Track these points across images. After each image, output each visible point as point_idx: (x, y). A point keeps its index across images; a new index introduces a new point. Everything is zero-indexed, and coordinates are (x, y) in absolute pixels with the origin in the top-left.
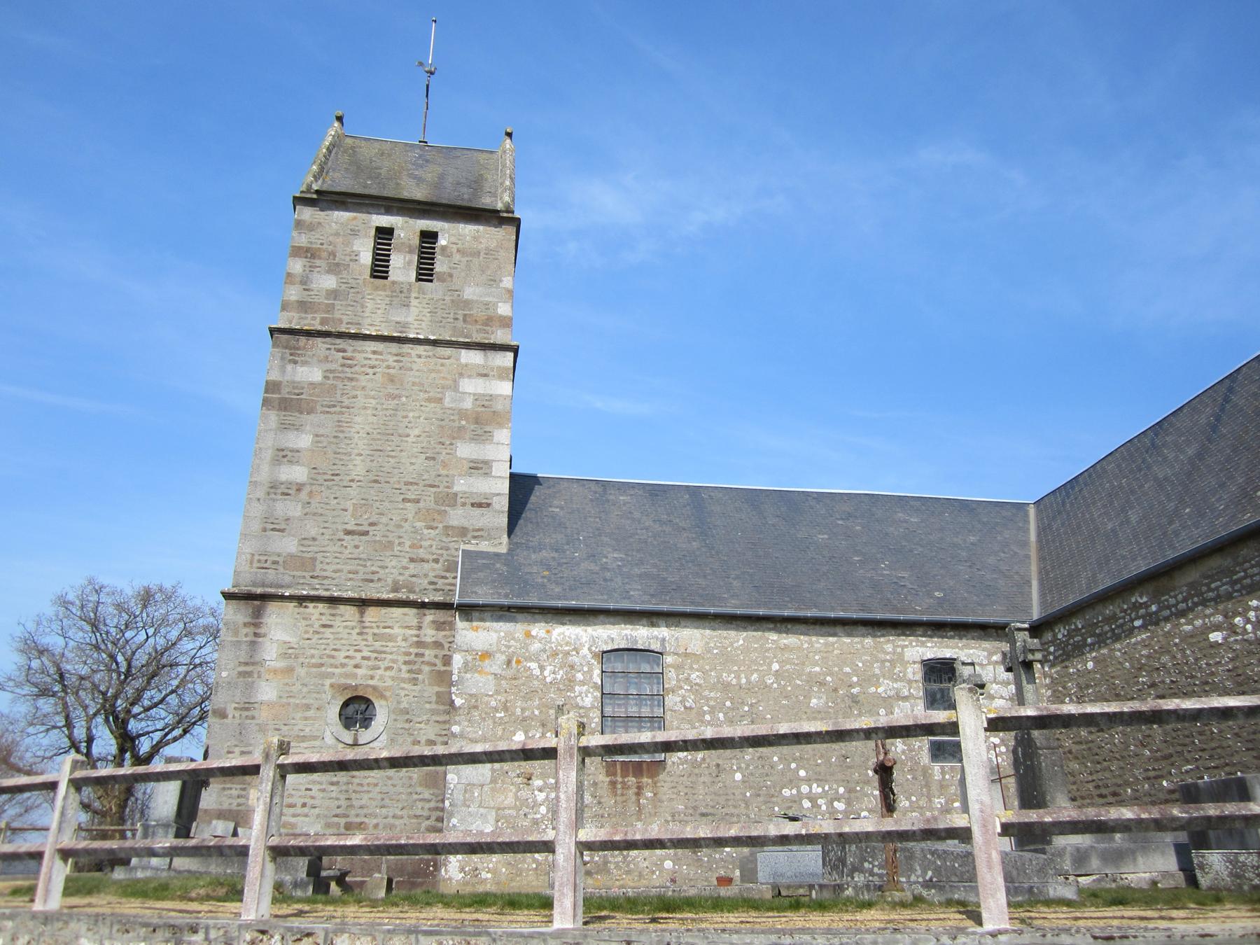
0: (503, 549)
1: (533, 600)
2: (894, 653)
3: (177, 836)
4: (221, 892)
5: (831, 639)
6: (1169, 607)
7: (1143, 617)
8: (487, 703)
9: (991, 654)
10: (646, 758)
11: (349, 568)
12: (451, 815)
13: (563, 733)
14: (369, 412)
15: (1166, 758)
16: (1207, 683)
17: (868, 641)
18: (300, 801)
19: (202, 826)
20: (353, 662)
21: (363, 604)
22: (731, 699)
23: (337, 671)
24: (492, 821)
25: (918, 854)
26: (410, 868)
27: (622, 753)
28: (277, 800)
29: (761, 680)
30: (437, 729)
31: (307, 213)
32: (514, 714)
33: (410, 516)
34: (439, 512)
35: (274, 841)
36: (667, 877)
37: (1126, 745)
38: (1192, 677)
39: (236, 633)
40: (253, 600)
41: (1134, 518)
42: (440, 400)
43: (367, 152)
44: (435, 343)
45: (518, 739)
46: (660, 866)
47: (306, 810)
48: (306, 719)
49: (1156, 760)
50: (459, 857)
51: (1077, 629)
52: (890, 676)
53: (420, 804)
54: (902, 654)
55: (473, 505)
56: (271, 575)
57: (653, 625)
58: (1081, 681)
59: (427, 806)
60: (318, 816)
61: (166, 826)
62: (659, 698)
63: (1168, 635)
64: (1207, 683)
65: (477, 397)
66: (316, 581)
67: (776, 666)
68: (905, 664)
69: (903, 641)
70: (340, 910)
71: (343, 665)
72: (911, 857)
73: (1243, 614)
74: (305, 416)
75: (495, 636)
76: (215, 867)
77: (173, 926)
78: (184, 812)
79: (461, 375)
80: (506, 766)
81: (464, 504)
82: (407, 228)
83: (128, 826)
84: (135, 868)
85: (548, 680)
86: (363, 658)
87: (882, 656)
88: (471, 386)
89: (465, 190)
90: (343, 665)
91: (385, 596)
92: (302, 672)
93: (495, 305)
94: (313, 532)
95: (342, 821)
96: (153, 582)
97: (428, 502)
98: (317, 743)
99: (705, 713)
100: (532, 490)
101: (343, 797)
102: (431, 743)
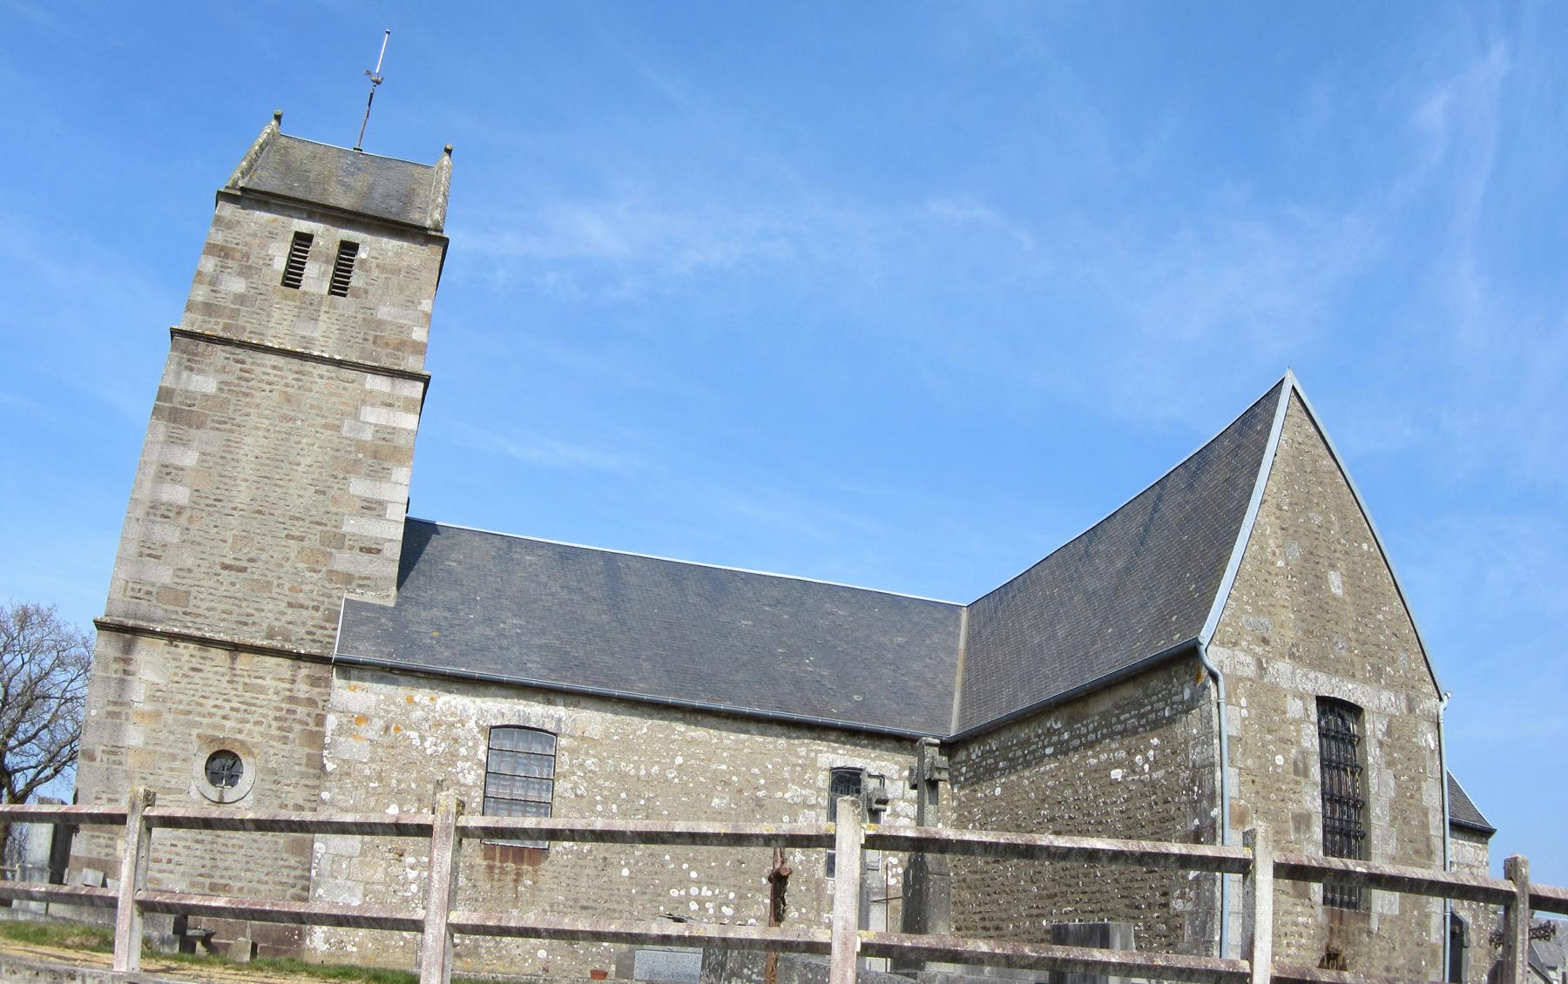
0: (390, 603)
1: (419, 663)
2: (807, 757)
3: (51, 881)
4: (94, 941)
5: (742, 736)
6: (1079, 737)
7: (1054, 745)
8: (360, 772)
9: (902, 769)
10: (529, 844)
11: (223, 606)
12: (318, 885)
13: (441, 810)
14: (261, 433)
15: (1049, 897)
16: (1100, 823)
17: (782, 742)
18: (165, 857)
19: (74, 873)
20: (221, 712)
21: (235, 648)
22: (628, 791)
23: (205, 720)
24: (360, 896)
25: (798, 965)
26: (274, 935)
27: (503, 837)
28: (143, 853)
29: (662, 773)
30: (306, 793)
31: (228, 210)
32: (388, 785)
33: (292, 555)
34: (325, 554)
35: (141, 896)
36: (539, 965)
37: (1017, 878)
38: (1089, 815)
39: (106, 668)
40: (125, 632)
41: (1060, 634)
42: (337, 428)
43: (299, 154)
44: (340, 364)
45: (392, 813)
46: (534, 955)
47: (171, 866)
48: (172, 769)
49: (1042, 898)
50: (325, 928)
51: (991, 751)
52: (790, 778)
53: (285, 871)
54: (815, 759)
55: (361, 549)
56: (144, 607)
57: (549, 703)
58: (987, 807)
59: (293, 873)
60: (183, 874)
61: (41, 870)
62: (549, 783)
63: (1074, 767)
64: (1100, 823)
65: (378, 429)
66: (188, 618)
67: (679, 760)
68: (816, 769)
69: (820, 746)
70: (206, 971)
71: (211, 715)
72: (791, 966)
73: (1144, 753)
74: (194, 431)
75: (373, 698)
76: (87, 917)
77: (54, 971)
78: (57, 856)
79: (364, 402)
80: (377, 839)
81: (351, 548)
82: (327, 237)
83: (7, 866)
84: (16, 911)
85: (429, 752)
86: (232, 709)
87: (793, 760)
88: (373, 416)
89: (393, 203)
90: (211, 715)
91: (259, 643)
92: (169, 718)
93: (410, 329)
94: (190, 563)
95: (208, 881)
96: (31, 602)
97: (313, 541)
98: (182, 797)
99: (597, 802)
100: (428, 539)
101: (208, 856)
102: (299, 808)
